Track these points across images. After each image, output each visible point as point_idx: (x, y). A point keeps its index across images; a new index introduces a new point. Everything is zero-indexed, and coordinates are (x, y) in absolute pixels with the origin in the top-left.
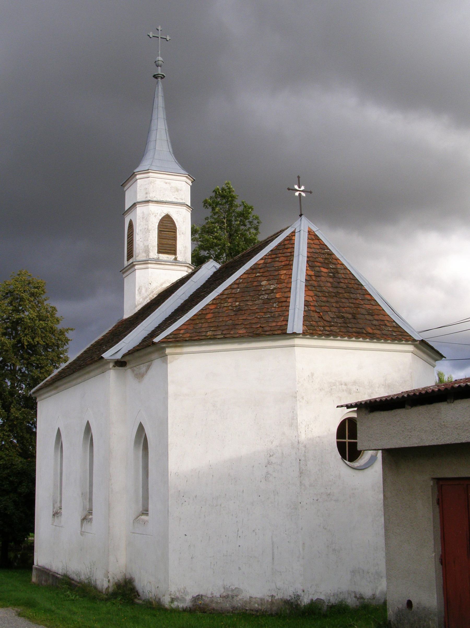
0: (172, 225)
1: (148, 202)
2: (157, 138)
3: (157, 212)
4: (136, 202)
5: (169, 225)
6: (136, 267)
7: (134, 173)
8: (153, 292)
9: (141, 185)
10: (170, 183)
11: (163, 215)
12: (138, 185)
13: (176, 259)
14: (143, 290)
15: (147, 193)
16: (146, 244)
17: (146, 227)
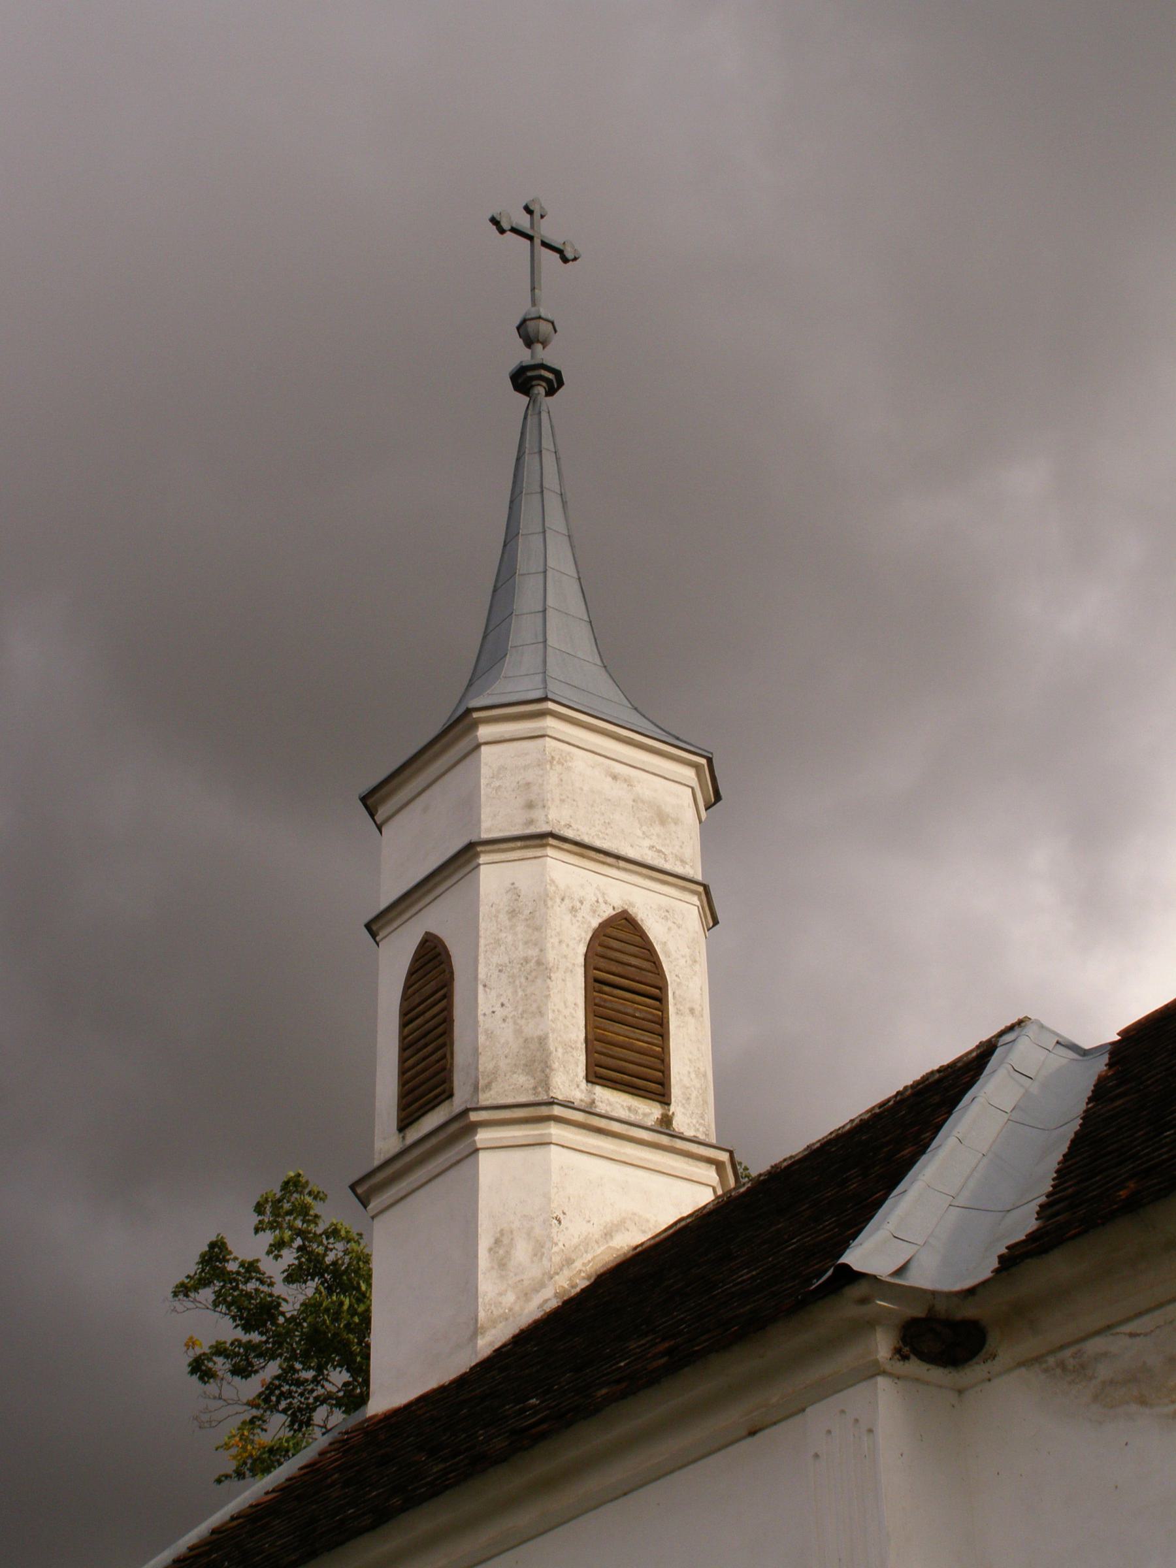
0: (645, 965)
1: (541, 839)
2: (550, 602)
3: (578, 899)
4: (474, 839)
5: (633, 961)
6: (483, 1136)
7: (469, 711)
8: (569, 1262)
9: (502, 768)
10: (628, 782)
11: (608, 912)
12: (484, 770)
13: (666, 1121)
14: (521, 1252)
15: (530, 806)
16: (531, 1029)
17: (533, 952)
